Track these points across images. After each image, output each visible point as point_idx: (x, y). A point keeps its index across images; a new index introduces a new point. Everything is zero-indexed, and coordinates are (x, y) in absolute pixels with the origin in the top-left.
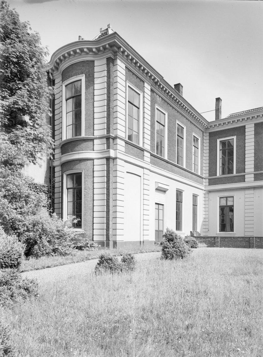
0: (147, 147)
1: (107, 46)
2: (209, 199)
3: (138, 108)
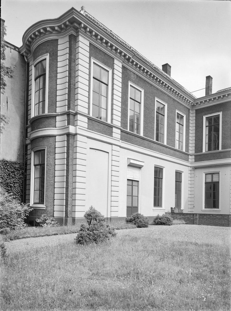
0: (117, 123)
1: (67, 23)
2: (194, 176)
3: (107, 85)
